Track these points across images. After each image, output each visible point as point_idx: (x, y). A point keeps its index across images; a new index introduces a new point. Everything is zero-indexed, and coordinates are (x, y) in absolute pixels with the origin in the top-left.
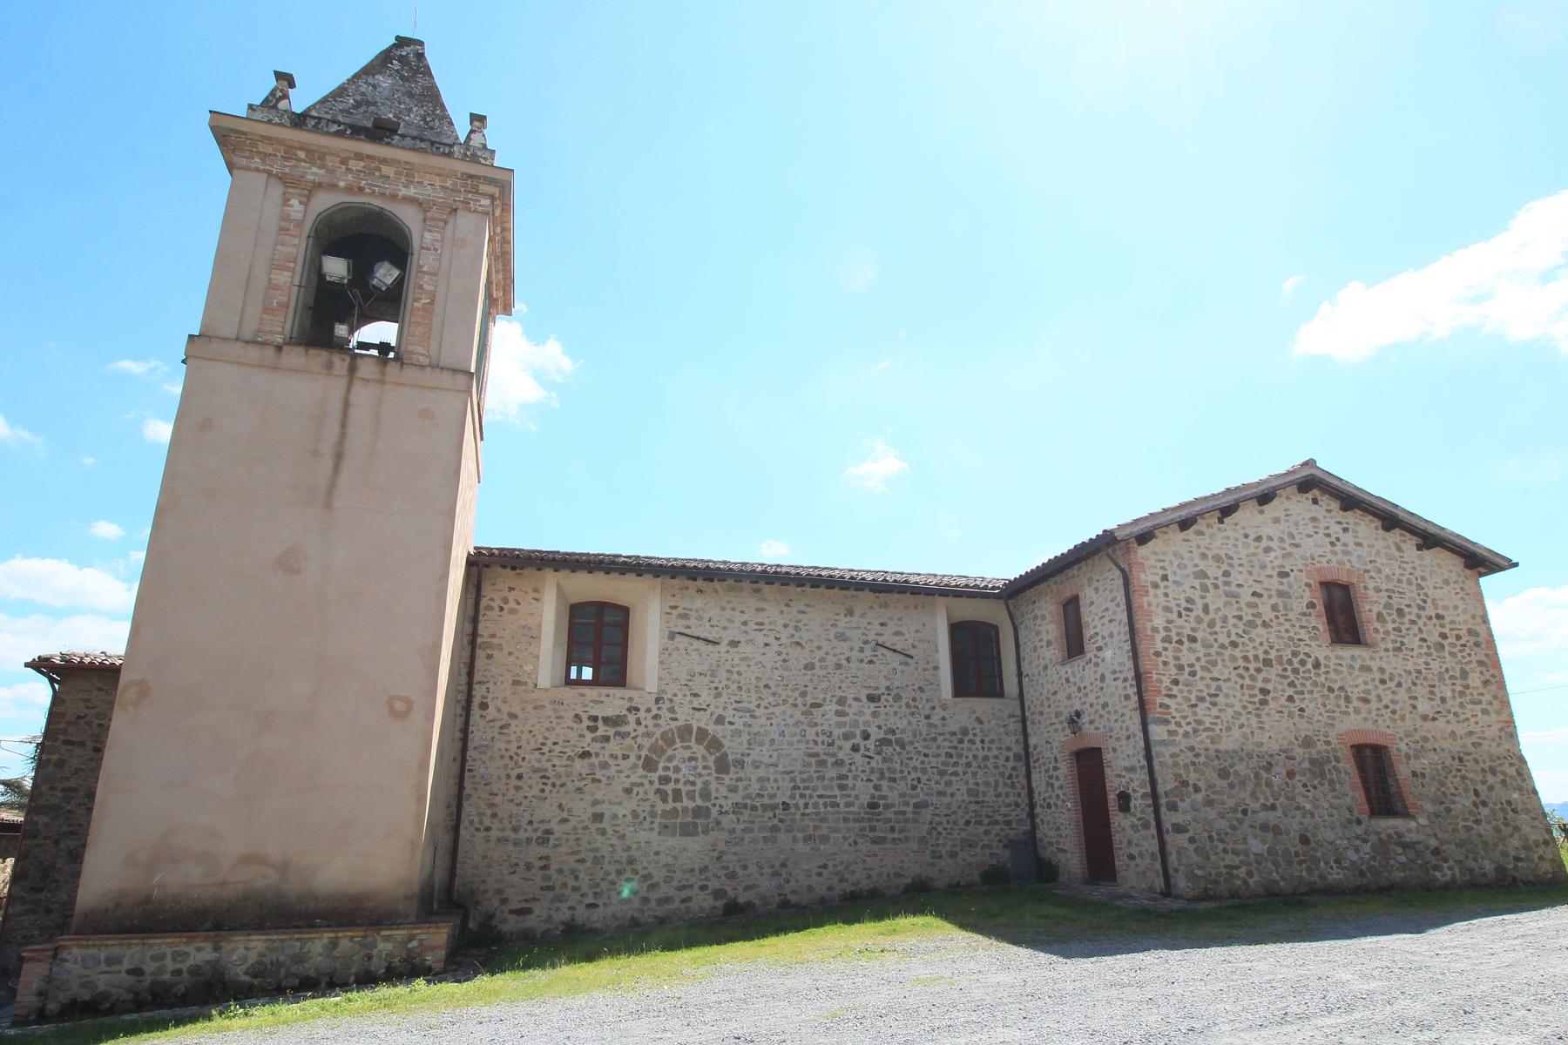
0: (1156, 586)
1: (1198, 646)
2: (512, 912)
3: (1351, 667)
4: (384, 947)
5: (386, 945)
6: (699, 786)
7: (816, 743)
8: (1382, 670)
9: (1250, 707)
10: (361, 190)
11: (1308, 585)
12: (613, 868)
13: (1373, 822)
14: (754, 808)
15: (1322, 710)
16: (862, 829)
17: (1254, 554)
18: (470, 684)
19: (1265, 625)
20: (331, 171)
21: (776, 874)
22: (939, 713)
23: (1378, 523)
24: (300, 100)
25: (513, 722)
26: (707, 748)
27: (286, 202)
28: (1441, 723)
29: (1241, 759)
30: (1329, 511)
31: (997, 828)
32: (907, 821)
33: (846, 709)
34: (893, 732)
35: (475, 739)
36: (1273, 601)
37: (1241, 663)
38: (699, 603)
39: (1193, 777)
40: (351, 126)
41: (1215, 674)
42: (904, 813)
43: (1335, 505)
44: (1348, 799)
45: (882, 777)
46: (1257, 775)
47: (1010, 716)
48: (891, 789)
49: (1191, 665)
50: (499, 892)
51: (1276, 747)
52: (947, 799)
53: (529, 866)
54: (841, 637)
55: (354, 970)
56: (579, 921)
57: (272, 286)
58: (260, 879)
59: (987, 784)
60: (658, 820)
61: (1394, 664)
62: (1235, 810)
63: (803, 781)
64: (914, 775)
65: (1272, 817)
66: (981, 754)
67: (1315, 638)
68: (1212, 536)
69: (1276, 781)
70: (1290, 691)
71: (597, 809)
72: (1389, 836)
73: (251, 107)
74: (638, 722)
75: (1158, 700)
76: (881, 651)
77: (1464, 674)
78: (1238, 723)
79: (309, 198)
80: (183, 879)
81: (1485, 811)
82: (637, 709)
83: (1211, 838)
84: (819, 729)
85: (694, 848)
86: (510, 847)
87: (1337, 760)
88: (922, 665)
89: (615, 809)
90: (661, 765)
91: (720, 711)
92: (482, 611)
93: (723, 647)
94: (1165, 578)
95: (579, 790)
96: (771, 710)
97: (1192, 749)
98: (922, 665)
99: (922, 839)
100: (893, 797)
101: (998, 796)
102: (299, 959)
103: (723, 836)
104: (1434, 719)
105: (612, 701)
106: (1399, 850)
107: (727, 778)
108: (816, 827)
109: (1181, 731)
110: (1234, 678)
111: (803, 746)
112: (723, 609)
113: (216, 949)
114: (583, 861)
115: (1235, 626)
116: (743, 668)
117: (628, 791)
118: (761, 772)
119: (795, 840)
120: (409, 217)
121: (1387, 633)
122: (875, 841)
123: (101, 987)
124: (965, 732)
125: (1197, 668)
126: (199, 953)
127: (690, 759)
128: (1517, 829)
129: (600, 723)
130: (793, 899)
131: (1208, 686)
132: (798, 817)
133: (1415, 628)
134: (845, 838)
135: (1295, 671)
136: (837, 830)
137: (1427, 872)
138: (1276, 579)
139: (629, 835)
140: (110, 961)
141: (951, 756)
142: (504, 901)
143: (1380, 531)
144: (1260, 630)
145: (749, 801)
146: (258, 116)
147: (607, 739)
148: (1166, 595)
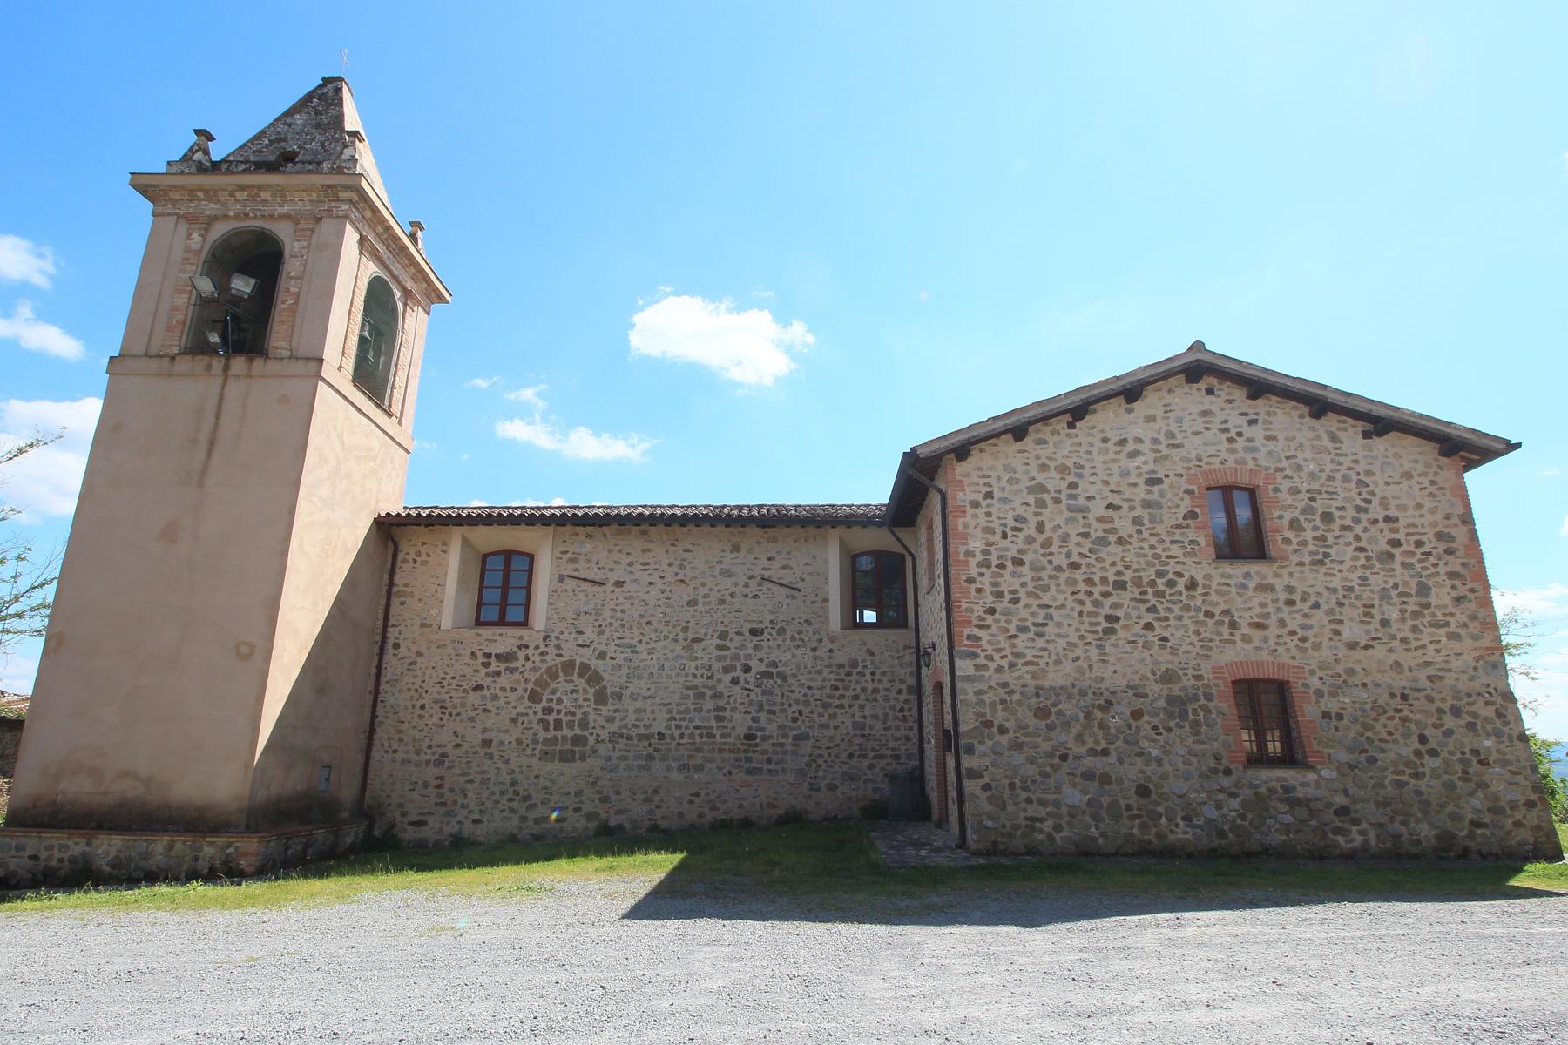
0: (976, 505)
1: (1025, 570)
2: (410, 823)
3: (1243, 586)
4: (208, 851)
5: (211, 848)
6: (579, 716)
7: (695, 676)
8: (1290, 589)
9: (1090, 637)
10: (247, 215)
11: (1188, 492)
12: (497, 789)
13: (1249, 772)
14: (629, 738)
15: (1195, 638)
16: (738, 760)
17: (1114, 461)
18: (385, 626)
19: (1120, 541)
20: (224, 205)
21: (647, 800)
22: (827, 645)
23: (1305, 410)
24: (218, 152)
25: (419, 660)
26: (588, 682)
27: (189, 236)
28: (1379, 652)
29: (1070, 697)
30: (1230, 402)
31: (883, 762)
32: (786, 752)
33: (728, 643)
34: (775, 665)
35: (388, 674)
36: (1136, 513)
37: (1082, 587)
38: (588, 547)
39: (999, 717)
40: (255, 163)
41: (1045, 601)
42: (782, 745)
43: (1239, 394)
44: (1216, 745)
45: (761, 709)
46: (1088, 715)
47: (906, 647)
48: (770, 721)
49: (1014, 592)
50: (401, 805)
51: (1124, 683)
52: (831, 732)
53: (426, 785)
54: (727, 573)
55: (185, 868)
56: (466, 834)
57: (174, 309)
58: (131, 790)
59: (875, 717)
60: (539, 747)
61: (1312, 581)
62: (1050, 755)
63: (679, 712)
64: (795, 707)
65: (1099, 764)
66: (870, 687)
67: (1193, 554)
68: (1058, 444)
69: (1114, 722)
70: (1149, 618)
71: (487, 736)
72: (1271, 790)
73: (169, 164)
74: (527, 659)
75: (966, 632)
76: (767, 585)
77: (1423, 590)
78: (1071, 655)
79: (206, 230)
80: (78, 789)
81: (1431, 763)
82: (527, 647)
83: (1012, 786)
84: (699, 662)
85: (568, 775)
86: (412, 768)
87: (1209, 697)
88: (811, 597)
89: (502, 736)
90: (545, 698)
91: (603, 647)
92: (399, 564)
93: (609, 588)
94: (989, 495)
95: (472, 719)
96: (653, 645)
97: (1005, 685)
98: (811, 597)
99: (801, 773)
100: (771, 729)
101: (886, 729)
102: (146, 856)
103: (598, 763)
104: (1367, 647)
105: (504, 640)
106: (1284, 807)
107: (604, 710)
108: (691, 757)
109: (992, 666)
110: (1070, 603)
111: (682, 679)
112: (610, 551)
113: (88, 844)
114: (471, 781)
115: (1078, 544)
116: (627, 606)
117: (514, 720)
118: (639, 704)
119: (669, 768)
120: (283, 231)
121: (1304, 543)
122: (749, 772)
123: (12, 868)
124: (854, 664)
125: (1022, 594)
126: (75, 846)
127: (572, 692)
128: (1482, 785)
129: (493, 660)
130: (663, 824)
131: (1034, 615)
132: (673, 746)
133: (1350, 536)
134: (719, 768)
135: (1159, 594)
136: (711, 760)
137: (1324, 835)
138: (1143, 487)
139: (513, 760)
140: (20, 848)
141: (837, 688)
142: (404, 814)
143: (1307, 419)
144: (1114, 548)
145: (625, 731)
146: (174, 170)
147: (498, 674)
148: (989, 514)
